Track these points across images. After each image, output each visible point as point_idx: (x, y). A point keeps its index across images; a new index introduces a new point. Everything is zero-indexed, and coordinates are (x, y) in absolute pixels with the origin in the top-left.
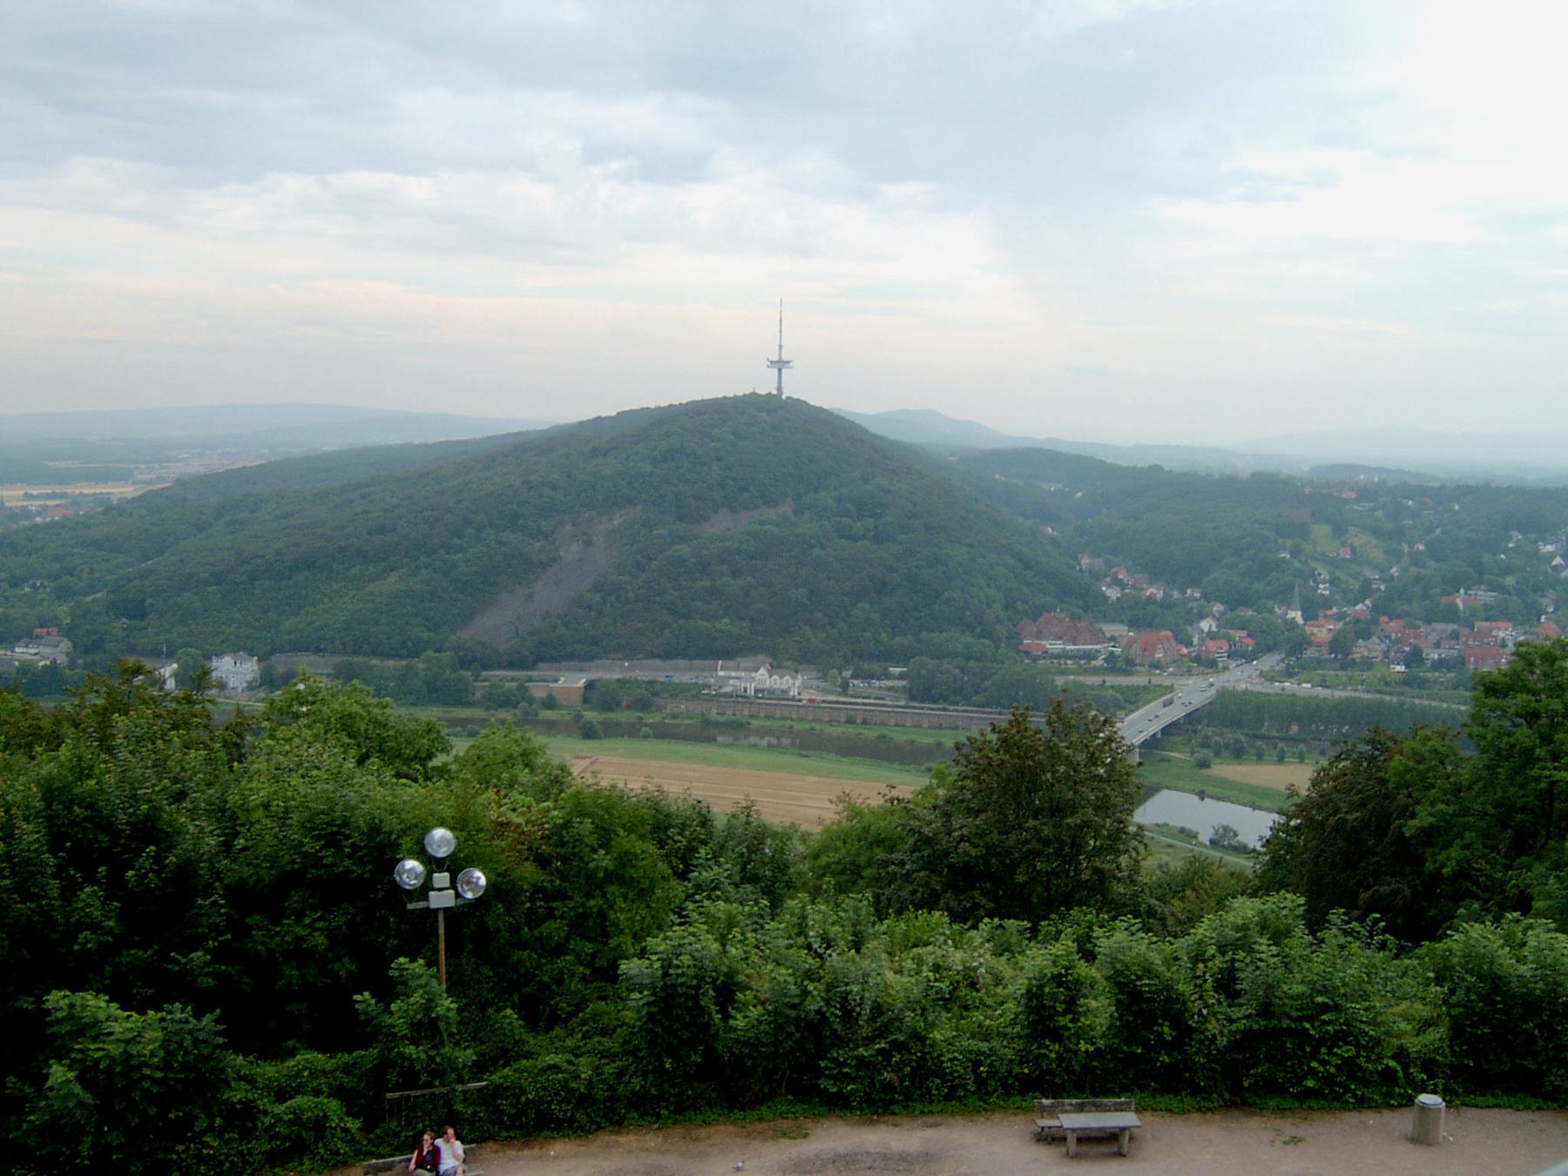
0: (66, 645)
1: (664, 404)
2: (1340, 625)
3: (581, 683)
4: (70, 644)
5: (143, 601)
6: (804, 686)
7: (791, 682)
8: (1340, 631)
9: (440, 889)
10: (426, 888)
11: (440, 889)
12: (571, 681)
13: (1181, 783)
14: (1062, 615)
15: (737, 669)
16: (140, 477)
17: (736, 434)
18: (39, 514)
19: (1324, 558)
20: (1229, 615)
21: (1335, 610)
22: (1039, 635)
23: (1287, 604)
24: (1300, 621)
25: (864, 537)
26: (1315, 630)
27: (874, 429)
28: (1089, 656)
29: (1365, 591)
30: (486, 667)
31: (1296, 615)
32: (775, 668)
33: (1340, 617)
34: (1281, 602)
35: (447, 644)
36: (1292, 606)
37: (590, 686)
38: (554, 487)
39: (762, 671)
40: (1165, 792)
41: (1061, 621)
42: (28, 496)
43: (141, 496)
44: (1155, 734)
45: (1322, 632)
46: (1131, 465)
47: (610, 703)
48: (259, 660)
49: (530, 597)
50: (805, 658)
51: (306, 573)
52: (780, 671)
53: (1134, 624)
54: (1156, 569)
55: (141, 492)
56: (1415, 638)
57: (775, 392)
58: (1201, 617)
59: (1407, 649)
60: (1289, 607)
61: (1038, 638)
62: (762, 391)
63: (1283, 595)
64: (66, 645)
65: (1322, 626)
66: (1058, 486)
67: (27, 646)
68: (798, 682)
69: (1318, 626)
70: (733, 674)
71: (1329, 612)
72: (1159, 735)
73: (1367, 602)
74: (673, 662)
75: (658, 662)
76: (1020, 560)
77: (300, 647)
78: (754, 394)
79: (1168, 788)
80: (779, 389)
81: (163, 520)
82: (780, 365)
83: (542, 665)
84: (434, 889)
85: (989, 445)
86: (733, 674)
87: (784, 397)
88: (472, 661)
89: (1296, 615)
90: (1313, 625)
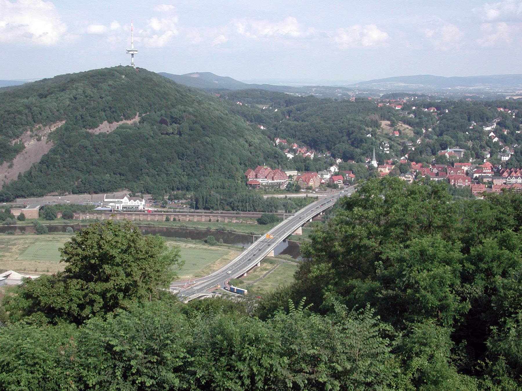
26: (382, 169)
27: (178, 82)
31: (375, 163)
32: (132, 197)
39: (126, 198)
52: (134, 198)
54: (313, 145)
63: (368, 153)
73: (406, 156)
90: (382, 168)
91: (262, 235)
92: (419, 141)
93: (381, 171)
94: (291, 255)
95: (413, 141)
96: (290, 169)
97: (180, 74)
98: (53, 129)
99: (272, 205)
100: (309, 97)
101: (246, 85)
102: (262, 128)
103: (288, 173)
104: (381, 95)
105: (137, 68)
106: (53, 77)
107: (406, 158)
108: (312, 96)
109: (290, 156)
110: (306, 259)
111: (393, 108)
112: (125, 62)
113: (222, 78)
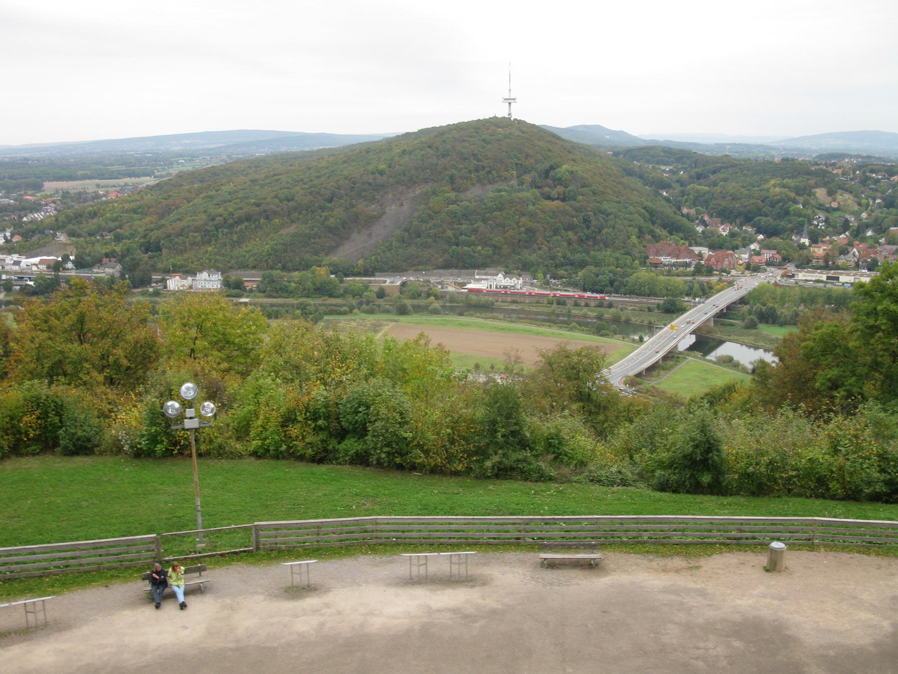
0: (119, 267)
1: (444, 124)
2: (830, 246)
3: (398, 284)
4: (121, 267)
5: (160, 242)
6: (525, 283)
7: (516, 281)
8: (830, 250)
9: (191, 418)
10: (181, 418)
11: (191, 418)
12: (391, 282)
13: (740, 338)
14: (671, 242)
15: (486, 274)
16: (158, 174)
17: (484, 141)
18: (104, 195)
19: (821, 207)
20: (768, 241)
21: (828, 238)
22: (657, 253)
23: (800, 234)
24: (807, 243)
25: (557, 199)
26: (816, 250)
27: (564, 136)
28: (687, 265)
29: (846, 226)
30: (347, 275)
31: (806, 241)
32: (507, 274)
33: (831, 242)
34: (797, 233)
35: (323, 262)
36: (804, 236)
37: (404, 284)
38: (382, 173)
39: (500, 275)
40: (728, 343)
41: (684, 244)
42: (98, 186)
43: (157, 184)
44: (722, 310)
45: (819, 251)
46: (768, 158)
47: (416, 295)
48: (222, 274)
49: (370, 235)
50: (525, 268)
51: (246, 223)
52: (510, 275)
53: (711, 247)
54: (726, 216)
55: (157, 182)
56: (873, 254)
57: (507, 116)
58: (752, 243)
59: (869, 260)
60: (801, 236)
61: (657, 255)
62: (499, 116)
63: (798, 230)
64: (119, 267)
65: (820, 247)
66: (671, 167)
67: (99, 269)
68: (521, 281)
69: (817, 247)
70: (484, 277)
71: (824, 239)
72: (725, 311)
73: (847, 233)
74: (450, 270)
75: (442, 271)
76: (647, 211)
77: (244, 266)
78: (495, 117)
79: (730, 341)
80: (510, 114)
81: (169, 196)
82: (510, 101)
83: (377, 274)
84: (186, 418)
85: (631, 145)
86: (484, 277)
87: (512, 119)
88: (343, 271)
89: (806, 241)
90: (815, 247)
91: (665, 325)
92: (864, 215)
93: (814, 252)
94: (700, 352)
95: (857, 214)
96: (698, 244)
97: (564, 126)
98: (418, 192)
99: (675, 293)
100: (723, 156)
101: (636, 138)
102: (665, 193)
103: (697, 249)
104: (814, 156)
105: (515, 120)
106: (416, 131)
107: (847, 236)
108: (727, 156)
109: (700, 229)
110: (688, 473)
111: (831, 172)
112: (501, 112)
113: (615, 133)
